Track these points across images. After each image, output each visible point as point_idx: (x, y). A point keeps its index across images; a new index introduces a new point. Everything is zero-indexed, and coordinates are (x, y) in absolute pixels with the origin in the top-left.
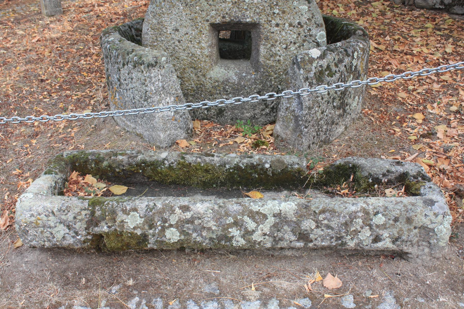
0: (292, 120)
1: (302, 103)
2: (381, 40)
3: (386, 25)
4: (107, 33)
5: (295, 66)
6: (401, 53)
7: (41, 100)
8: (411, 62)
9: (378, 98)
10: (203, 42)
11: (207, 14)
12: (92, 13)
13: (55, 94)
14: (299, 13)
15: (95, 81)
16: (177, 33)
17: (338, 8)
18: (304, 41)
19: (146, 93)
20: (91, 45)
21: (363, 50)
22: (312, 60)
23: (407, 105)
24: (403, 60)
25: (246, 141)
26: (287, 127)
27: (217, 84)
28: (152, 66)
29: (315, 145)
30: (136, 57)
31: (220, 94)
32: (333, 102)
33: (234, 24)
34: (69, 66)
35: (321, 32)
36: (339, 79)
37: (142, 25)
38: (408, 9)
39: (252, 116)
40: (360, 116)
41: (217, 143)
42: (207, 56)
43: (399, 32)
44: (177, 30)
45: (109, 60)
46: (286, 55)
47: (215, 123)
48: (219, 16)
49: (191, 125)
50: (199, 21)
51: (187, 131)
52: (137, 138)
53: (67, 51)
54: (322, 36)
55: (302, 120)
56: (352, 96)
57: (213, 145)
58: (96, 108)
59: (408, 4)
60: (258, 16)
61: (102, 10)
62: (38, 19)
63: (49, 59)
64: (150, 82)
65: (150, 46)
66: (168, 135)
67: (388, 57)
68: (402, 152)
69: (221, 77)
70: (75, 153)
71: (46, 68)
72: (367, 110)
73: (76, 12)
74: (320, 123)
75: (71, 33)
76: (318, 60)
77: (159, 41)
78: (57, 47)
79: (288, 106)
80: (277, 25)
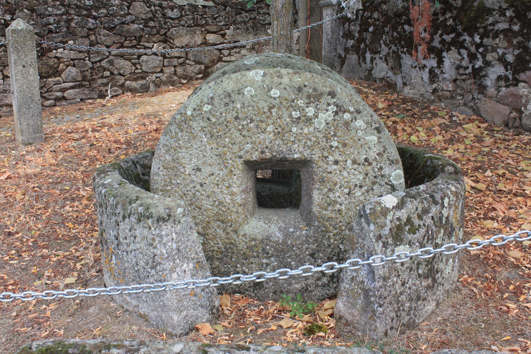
0: (360, 295)
1: (374, 272)
2: (480, 176)
3: (485, 155)
4: (102, 173)
5: (363, 220)
6: (508, 193)
7: (6, 262)
8: (524, 206)
9: (481, 259)
10: (234, 185)
11: (239, 148)
12: (84, 141)
13: (27, 253)
14: (366, 146)
15: (84, 236)
16: (198, 173)
17: (417, 134)
18: (374, 183)
19: (154, 257)
20: (80, 184)
21: (456, 194)
22: (385, 212)
23: (524, 268)
24: (512, 204)
25: (295, 324)
26: (353, 305)
27: (253, 243)
28: (164, 220)
29: (394, 331)
30: (140, 208)
31: (258, 257)
32: (418, 268)
33: (277, 161)
34: (48, 214)
35: (397, 171)
36: (424, 236)
37: (151, 160)
38: (513, 132)
39: (303, 288)
40: (457, 286)
41: (253, 327)
42: (240, 205)
43: (503, 165)
44: (199, 170)
45: (104, 211)
46: (349, 203)
47: (251, 298)
48: (257, 150)
49: (216, 302)
50: (228, 158)
51: (212, 311)
52: (140, 321)
53: (46, 193)
54: (398, 176)
55: (375, 296)
56: (444, 259)
57: (248, 331)
58: (83, 274)
59: (513, 127)
60: (309, 151)
61: (97, 137)
62: (10, 148)
63: (21, 204)
64: (160, 242)
65: (161, 191)
66: (184, 318)
67: (490, 200)
68: (522, 340)
69: (259, 233)
70: (50, 344)
71: (17, 216)
72: (466, 276)
73: (62, 139)
74: (400, 299)
75: (54, 168)
76: (394, 211)
77: (174, 184)
78: (34, 187)
79: (355, 275)
80: (336, 162)
